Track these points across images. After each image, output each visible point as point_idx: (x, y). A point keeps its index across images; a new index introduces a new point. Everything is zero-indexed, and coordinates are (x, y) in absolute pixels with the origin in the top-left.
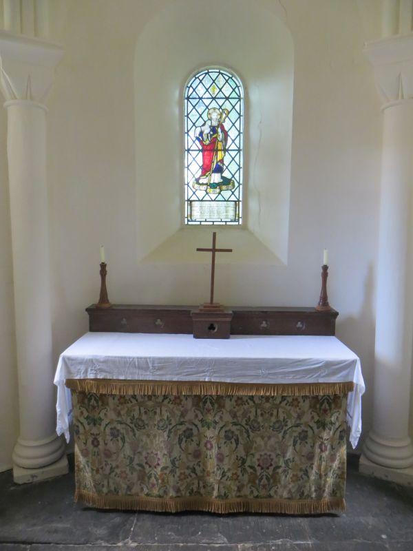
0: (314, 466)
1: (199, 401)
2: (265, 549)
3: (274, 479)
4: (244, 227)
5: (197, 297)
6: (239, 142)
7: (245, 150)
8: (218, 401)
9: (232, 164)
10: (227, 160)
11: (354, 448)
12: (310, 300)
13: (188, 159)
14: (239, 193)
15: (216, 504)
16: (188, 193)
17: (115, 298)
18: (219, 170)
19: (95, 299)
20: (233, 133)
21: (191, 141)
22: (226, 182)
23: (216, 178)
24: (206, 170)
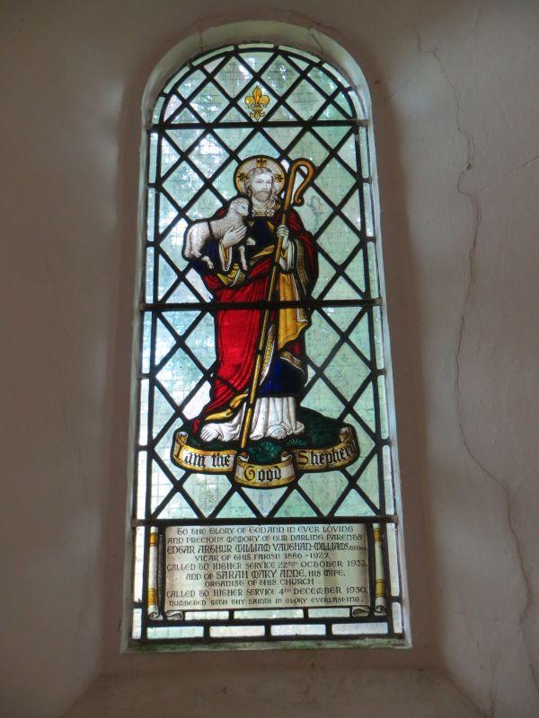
18: (288, 382)
20: (337, 242)
23: (272, 417)
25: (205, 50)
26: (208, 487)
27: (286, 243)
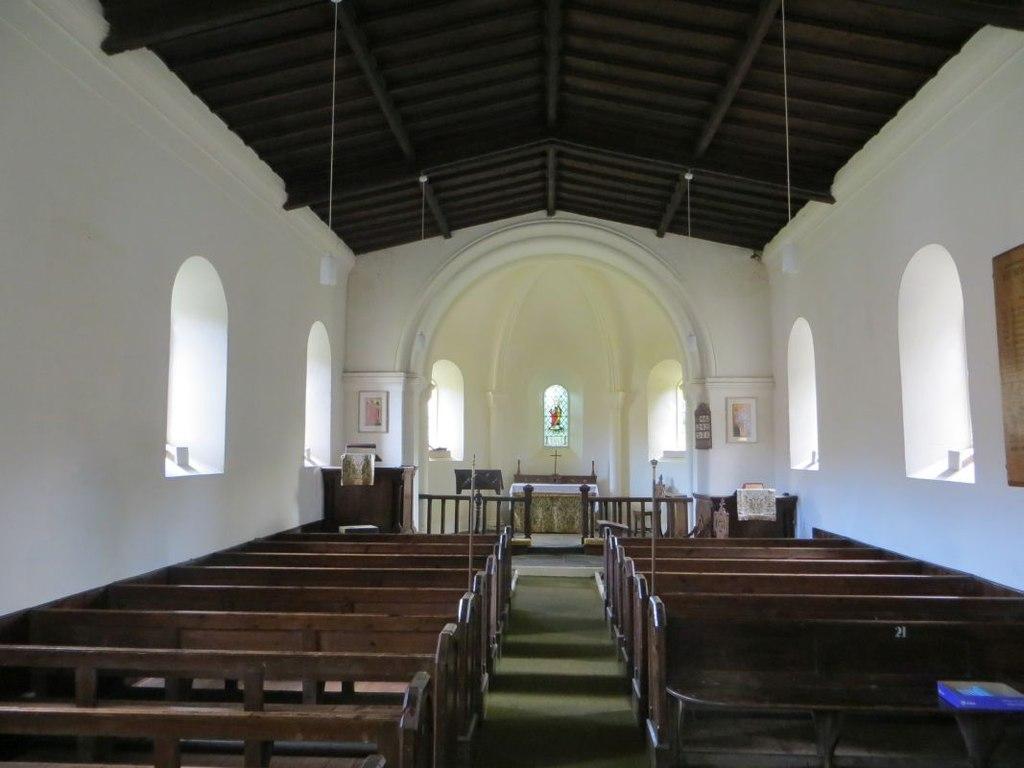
0: (551, 420)
1: (552, 498)
2: (383, 762)
3: (573, 523)
4: (568, 447)
5: (550, 472)
6: (566, 413)
7: (568, 417)
8: (557, 498)
9: (564, 421)
10: (561, 420)
11: (133, 686)
12: (590, 474)
13: (546, 419)
14: (566, 434)
15: (556, 530)
16: (546, 433)
17: (523, 472)
18: (558, 424)
19: (516, 473)
20: (563, 410)
21: (548, 414)
22: (561, 429)
23: (557, 427)
24: (553, 424)
25: (561, 473)
26: (551, 433)
27: (540, 516)
